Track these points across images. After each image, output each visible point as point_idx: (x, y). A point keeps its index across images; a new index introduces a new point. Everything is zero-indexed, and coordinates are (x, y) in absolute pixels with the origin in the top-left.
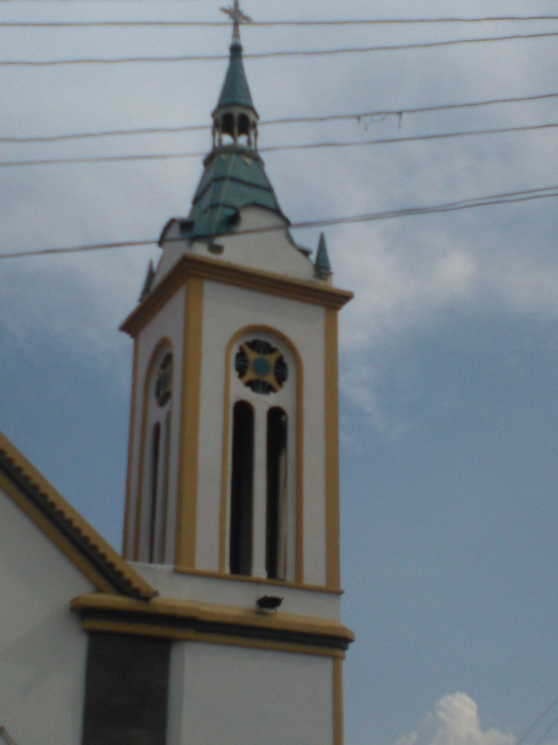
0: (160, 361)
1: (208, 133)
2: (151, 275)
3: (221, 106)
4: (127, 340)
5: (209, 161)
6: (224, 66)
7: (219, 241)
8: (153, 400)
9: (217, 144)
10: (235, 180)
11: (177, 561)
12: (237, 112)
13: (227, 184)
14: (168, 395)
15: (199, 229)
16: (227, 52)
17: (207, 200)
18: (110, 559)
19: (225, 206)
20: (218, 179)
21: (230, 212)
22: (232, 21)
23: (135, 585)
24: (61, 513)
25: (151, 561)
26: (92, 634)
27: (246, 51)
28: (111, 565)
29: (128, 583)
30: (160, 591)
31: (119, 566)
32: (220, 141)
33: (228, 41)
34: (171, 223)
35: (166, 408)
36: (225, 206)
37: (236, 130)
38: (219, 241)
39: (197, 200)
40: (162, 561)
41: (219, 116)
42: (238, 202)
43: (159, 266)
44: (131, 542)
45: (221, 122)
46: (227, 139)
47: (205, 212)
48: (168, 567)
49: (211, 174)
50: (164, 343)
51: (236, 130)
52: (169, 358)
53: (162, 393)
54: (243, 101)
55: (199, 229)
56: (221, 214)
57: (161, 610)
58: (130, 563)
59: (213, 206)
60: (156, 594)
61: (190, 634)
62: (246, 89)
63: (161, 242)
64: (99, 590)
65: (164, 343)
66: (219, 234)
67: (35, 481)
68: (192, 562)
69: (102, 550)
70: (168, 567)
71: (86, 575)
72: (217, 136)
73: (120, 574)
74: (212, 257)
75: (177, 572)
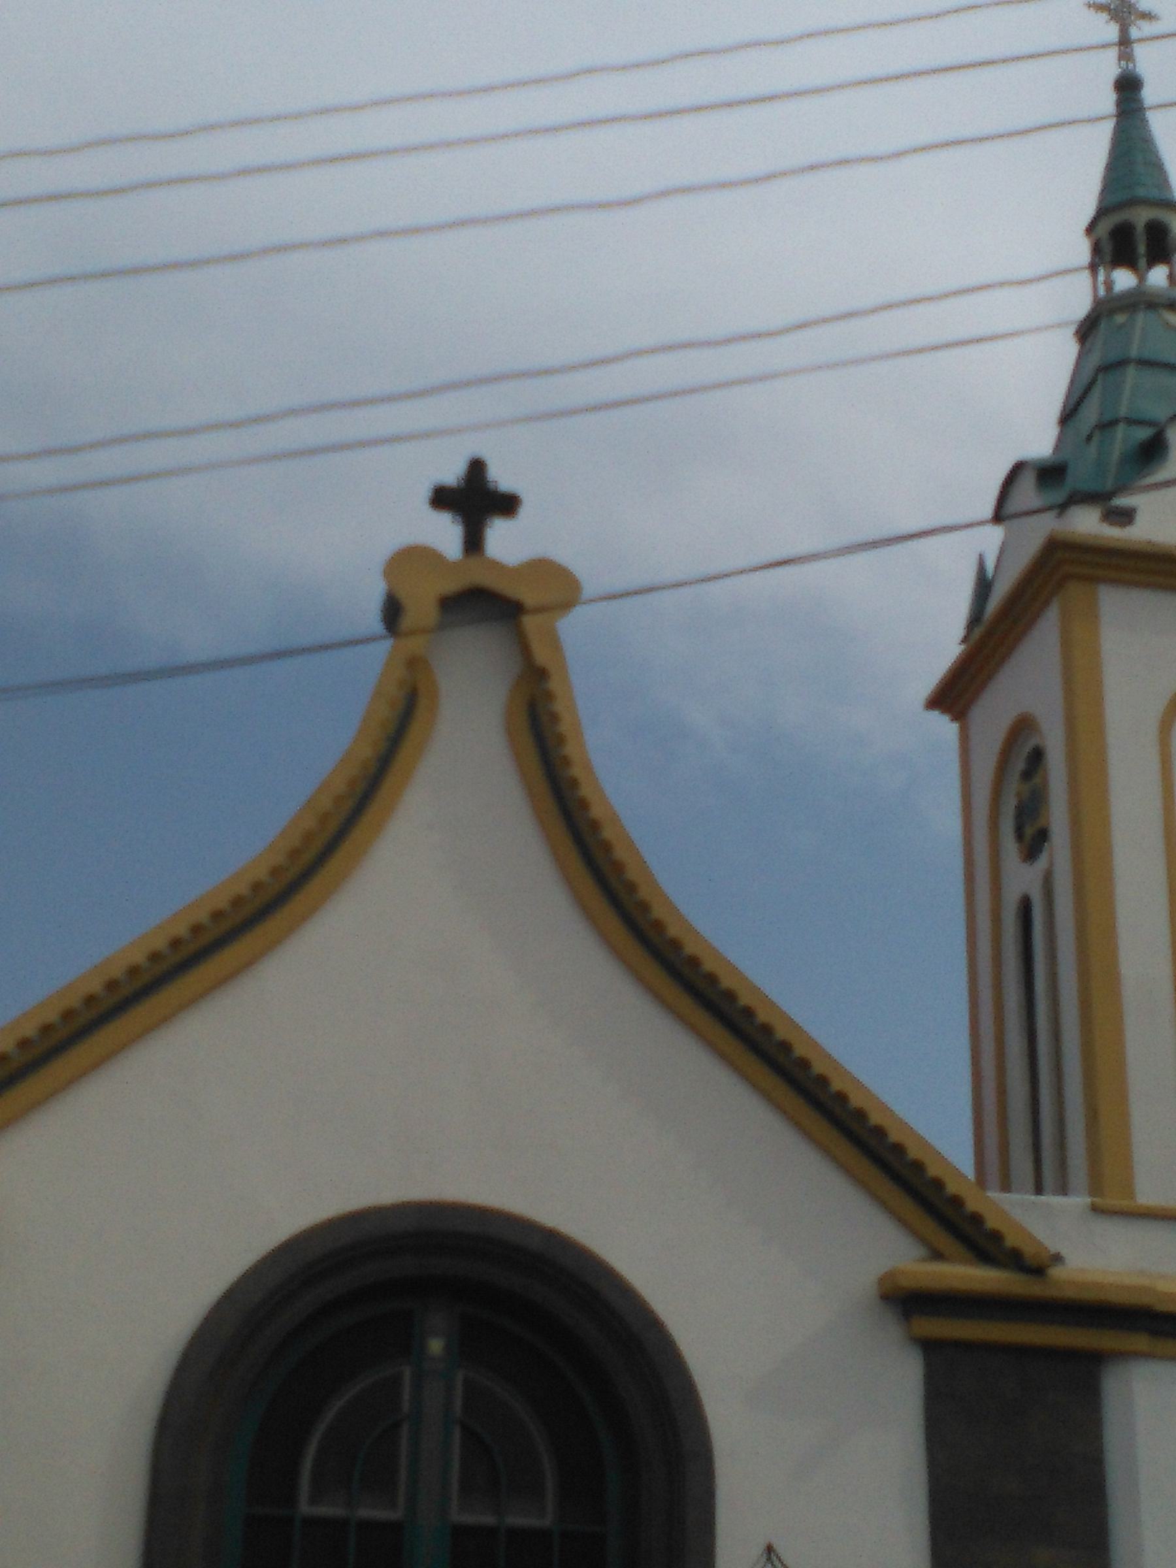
0: (1019, 765)
1: (1085, 278)
2: (983, 586)
3: (1102, 212)
4: (945, 728)
5: (1086, 331)
6: (1104, 133)
7: (1122, 501)
8: (1011, 848)
9: (1102, 292)
10: (1146, 363)
11: (1096, 1186)
12: (1141, 217)
13: (1131, 372)
14: (1043, 835)
15: (1079, 477)
16: (1107, 101)
17: (1090, 414)
18: (952, 1188)
19: (1132, 422)
20: (1113, 367)
21: (1143, 434)
22: (1111, 32)
23: (1011, 1241)
24: (842, 1097)
25: (1039, 1190)
26: (930, 1348)
27: (1150, 94)
28: (956, 1202)
29: (996, 1237)
30: (1064, 1252)
31: (973, 1204)
32: (1109, 285)
33: (1108, 67)
34: (1018, 469)
35: (1042, 863)
36: (1132, 422)
37: (1142, 262)
38: (1122, 501)
39: (1067, 417)
40: (1063, 1189)
41: (1104, 229)
42: (1160, 412)
43: (997, 567)
44: (992, 1155)
45: (1107, 248)
46: (1124, 279)
47: (1089, 438)
48: (1078, 1201)
49: (1095, 360)
50: (1023, 726)
51: (1142, 262)
52: (1037, 756)
53: (1029, 831)
54: (1154, 193)
55: (1079, 477)
56: (1125, 438)
57: (1070, 1293)
58: (994, 1195)
59: (1106, 426)
60: (1057, 1258)
61: (1141, 1342)
62: (1157, 167)
63: (998, 517)
64: (937, 1255)
65: (1023, 726)
66: (1122, 488)
67: (632, 874)
68: (1128, 1189)
69: (933, 1171)
70: (1078, 1201)
71: (903, 1223)
72: (1101, 278)
73: (977, 1219)
74: (1113, 533)
75: (1095, 1209)
